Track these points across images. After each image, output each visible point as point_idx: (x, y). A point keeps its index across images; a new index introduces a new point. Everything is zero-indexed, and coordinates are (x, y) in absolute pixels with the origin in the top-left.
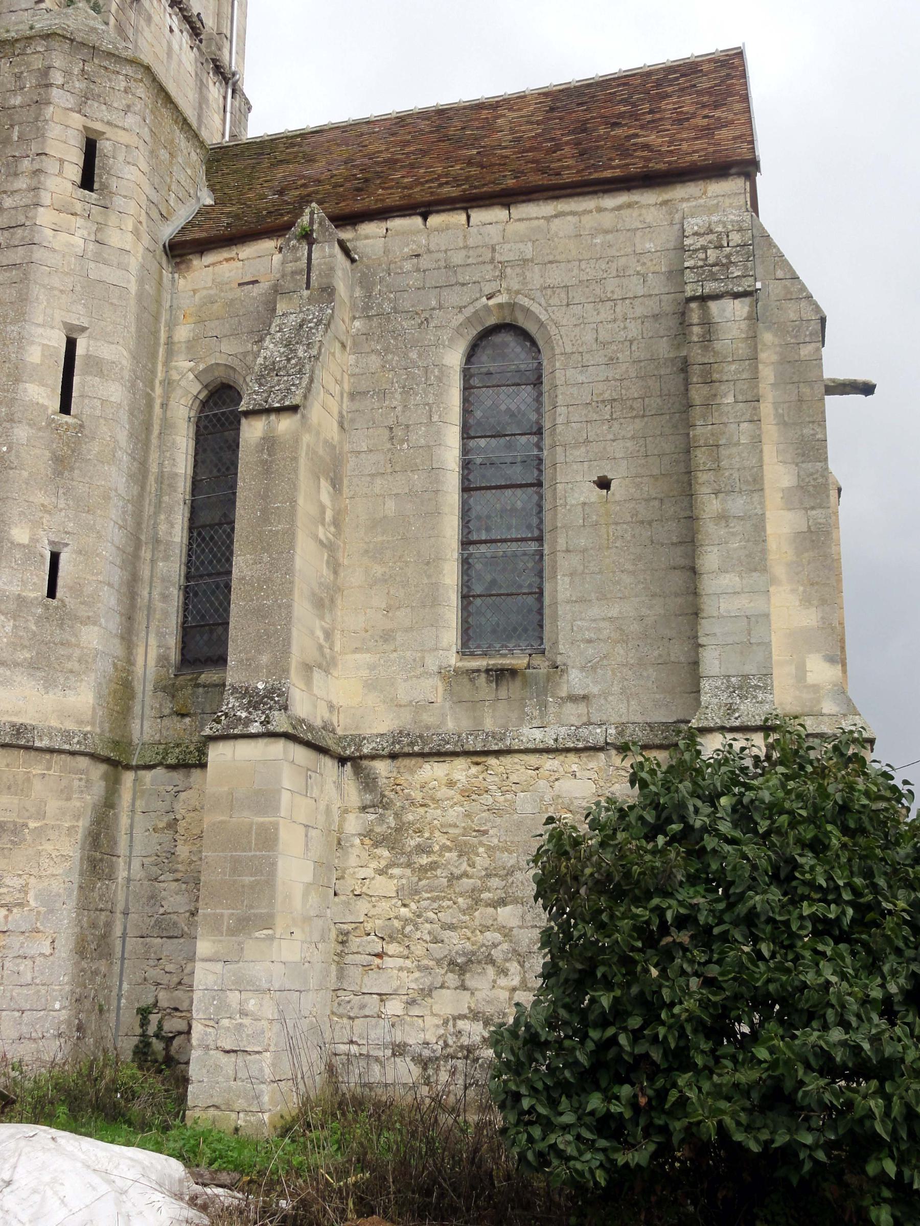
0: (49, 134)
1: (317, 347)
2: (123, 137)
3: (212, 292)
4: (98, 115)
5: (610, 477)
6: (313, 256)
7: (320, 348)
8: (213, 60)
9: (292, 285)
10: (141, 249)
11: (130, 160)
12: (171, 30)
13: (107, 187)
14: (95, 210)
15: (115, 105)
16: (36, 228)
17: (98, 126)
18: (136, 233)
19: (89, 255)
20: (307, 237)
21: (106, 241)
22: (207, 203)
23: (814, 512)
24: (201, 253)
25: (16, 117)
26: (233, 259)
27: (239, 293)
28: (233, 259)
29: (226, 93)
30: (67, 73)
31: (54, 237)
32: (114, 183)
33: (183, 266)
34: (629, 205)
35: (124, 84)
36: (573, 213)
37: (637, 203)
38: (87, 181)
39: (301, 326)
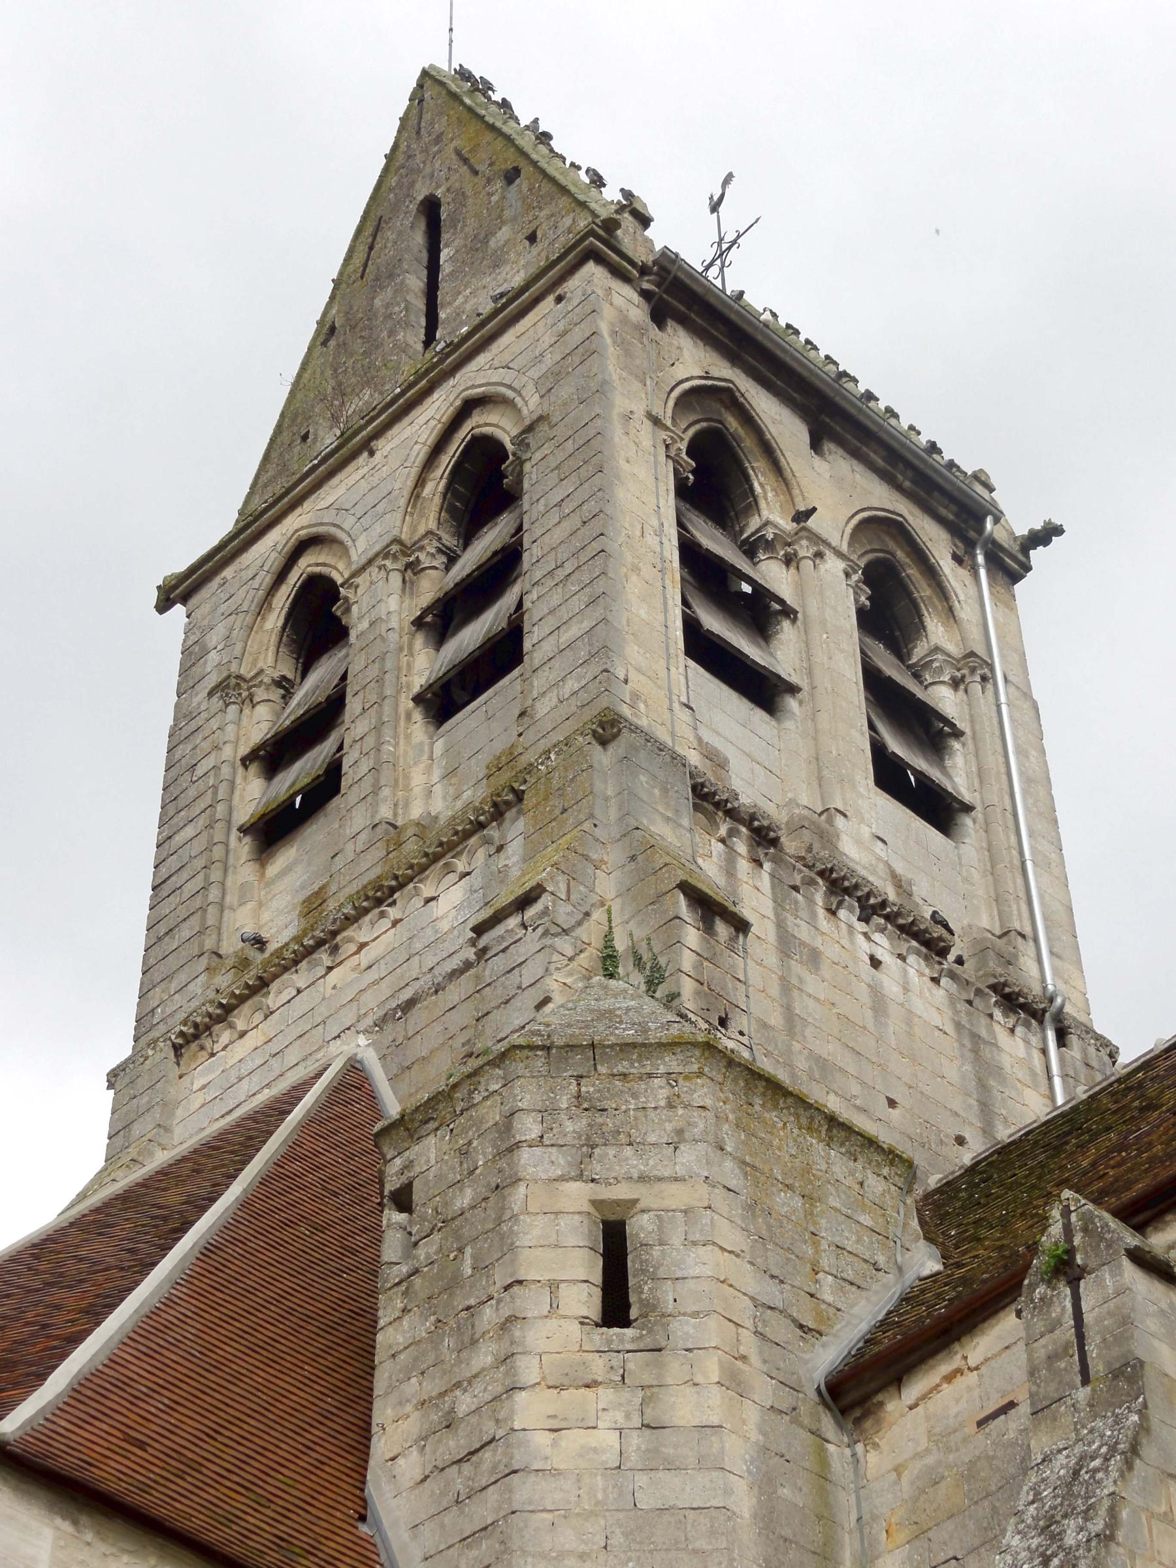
0: (524, 1241)
1: (1103, 1511)
2: (676, 1196)
3: (930, 1460)
4: (620, 1170)
6: (1085, 1307)
7: (1113, 1512)
8: (994, 988)
9: (1052, 1387)
10: (752, 1414)
11: (698, 1237)
12: (875, 963)
13: (654, 1308)
14: (634, 1362)
15: (652, 1138)
16: (513, 1438)
17: (622, 1192)
18: (734, 1383)
19: (634, 1459)
20: (1067, 1269)
21: (666, 1420)
22: (926, 1272)
24: (898, 1382)
25: (466, 1231)
26: (958, 1372)
27: (982, 1442)
28: (958, 1372)
29: (1044, 1040)
30: (547, 1112)
31: (555, 1444)
32: (667, 1294)
33: (868, 1424)
35: (664, 1093)
38: (616, 1308)
39: (1076, 1473)
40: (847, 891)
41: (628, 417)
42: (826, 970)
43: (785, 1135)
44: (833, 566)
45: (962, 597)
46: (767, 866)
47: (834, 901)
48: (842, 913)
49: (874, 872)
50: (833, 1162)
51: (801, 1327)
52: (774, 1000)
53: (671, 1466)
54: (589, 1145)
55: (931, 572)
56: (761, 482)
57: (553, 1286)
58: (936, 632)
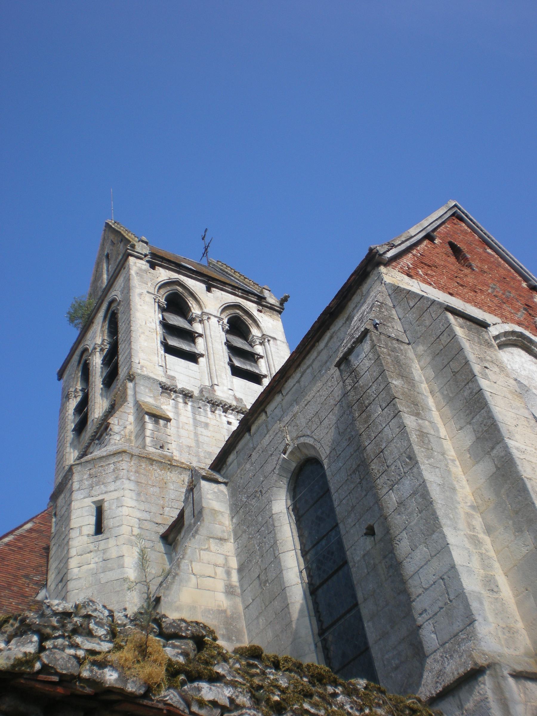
5: (372, 524)
17: (100, 498)
23: (495, 451)
30: (81, 481)
34: (331, 337)
36: (308, 367)
37: (334, 332)
38: (99, 529)
40: (218, 405)
41: (141, 294)
42: (211, 428)
43: (157, 472)
44: (214, 320)
45: (261, 321)
46: (190, 404)
47: (213, 409)
48: (217, 412)
49: (228, 399)
52: (192, 439)
53: (111, 569)
54: (92, 487)
55: (251, 316)
56: (191, 303)
58: (255, 331)
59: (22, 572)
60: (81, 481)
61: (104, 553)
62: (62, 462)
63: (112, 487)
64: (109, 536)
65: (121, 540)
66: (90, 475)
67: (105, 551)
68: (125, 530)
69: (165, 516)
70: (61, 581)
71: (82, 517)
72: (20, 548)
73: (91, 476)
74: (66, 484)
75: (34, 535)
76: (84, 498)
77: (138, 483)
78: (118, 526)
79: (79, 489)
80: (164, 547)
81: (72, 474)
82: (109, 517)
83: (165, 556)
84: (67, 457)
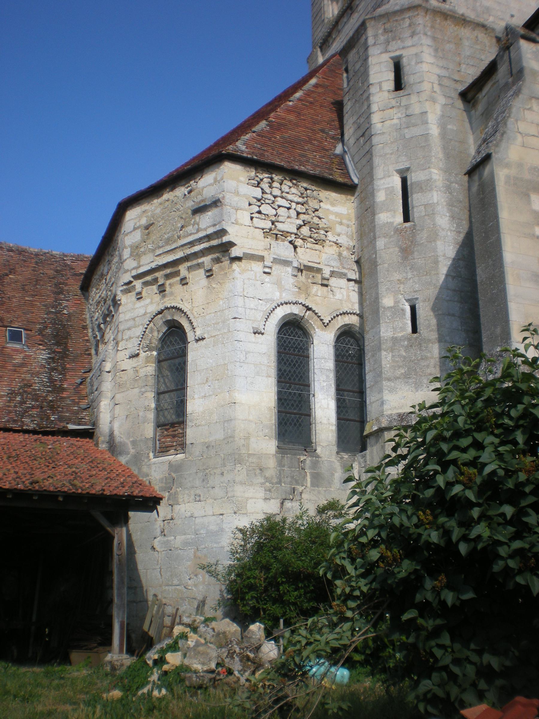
17: (397, 53)
30: (375, 36)
38: (399, 85)
43: (451, 28)
50: (465, 32)
51: (455, 80)
53: (415, 125)
54: (388, 42)
57: (380, 83)
59: (317, 127)
60: (375, 36)
61: (406, 109)
62: (319, 15)
63: (409, 42)
64: (410, 92)
65: (424, 96)
66: (385, 29)
67: (407, 107)
68: (426, 86)
69: (462, 73)
70: (363, 135)
71: (380, 74)
72: (311, 103)
73: (386, 31)
74: (359, 39)
75: (320, 90)
76: (381, 53)
77: (434, 39)
78: (419, 83)
79: (375, 44)
80: (463, 103)
81: (365, 29)
82: (409, 73)
83: (465, 114)
84: (325, 9)
